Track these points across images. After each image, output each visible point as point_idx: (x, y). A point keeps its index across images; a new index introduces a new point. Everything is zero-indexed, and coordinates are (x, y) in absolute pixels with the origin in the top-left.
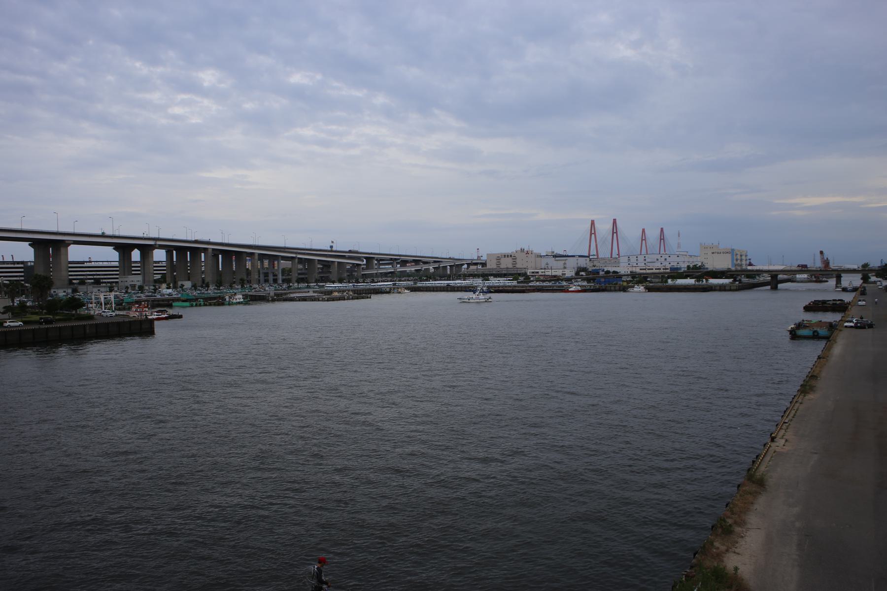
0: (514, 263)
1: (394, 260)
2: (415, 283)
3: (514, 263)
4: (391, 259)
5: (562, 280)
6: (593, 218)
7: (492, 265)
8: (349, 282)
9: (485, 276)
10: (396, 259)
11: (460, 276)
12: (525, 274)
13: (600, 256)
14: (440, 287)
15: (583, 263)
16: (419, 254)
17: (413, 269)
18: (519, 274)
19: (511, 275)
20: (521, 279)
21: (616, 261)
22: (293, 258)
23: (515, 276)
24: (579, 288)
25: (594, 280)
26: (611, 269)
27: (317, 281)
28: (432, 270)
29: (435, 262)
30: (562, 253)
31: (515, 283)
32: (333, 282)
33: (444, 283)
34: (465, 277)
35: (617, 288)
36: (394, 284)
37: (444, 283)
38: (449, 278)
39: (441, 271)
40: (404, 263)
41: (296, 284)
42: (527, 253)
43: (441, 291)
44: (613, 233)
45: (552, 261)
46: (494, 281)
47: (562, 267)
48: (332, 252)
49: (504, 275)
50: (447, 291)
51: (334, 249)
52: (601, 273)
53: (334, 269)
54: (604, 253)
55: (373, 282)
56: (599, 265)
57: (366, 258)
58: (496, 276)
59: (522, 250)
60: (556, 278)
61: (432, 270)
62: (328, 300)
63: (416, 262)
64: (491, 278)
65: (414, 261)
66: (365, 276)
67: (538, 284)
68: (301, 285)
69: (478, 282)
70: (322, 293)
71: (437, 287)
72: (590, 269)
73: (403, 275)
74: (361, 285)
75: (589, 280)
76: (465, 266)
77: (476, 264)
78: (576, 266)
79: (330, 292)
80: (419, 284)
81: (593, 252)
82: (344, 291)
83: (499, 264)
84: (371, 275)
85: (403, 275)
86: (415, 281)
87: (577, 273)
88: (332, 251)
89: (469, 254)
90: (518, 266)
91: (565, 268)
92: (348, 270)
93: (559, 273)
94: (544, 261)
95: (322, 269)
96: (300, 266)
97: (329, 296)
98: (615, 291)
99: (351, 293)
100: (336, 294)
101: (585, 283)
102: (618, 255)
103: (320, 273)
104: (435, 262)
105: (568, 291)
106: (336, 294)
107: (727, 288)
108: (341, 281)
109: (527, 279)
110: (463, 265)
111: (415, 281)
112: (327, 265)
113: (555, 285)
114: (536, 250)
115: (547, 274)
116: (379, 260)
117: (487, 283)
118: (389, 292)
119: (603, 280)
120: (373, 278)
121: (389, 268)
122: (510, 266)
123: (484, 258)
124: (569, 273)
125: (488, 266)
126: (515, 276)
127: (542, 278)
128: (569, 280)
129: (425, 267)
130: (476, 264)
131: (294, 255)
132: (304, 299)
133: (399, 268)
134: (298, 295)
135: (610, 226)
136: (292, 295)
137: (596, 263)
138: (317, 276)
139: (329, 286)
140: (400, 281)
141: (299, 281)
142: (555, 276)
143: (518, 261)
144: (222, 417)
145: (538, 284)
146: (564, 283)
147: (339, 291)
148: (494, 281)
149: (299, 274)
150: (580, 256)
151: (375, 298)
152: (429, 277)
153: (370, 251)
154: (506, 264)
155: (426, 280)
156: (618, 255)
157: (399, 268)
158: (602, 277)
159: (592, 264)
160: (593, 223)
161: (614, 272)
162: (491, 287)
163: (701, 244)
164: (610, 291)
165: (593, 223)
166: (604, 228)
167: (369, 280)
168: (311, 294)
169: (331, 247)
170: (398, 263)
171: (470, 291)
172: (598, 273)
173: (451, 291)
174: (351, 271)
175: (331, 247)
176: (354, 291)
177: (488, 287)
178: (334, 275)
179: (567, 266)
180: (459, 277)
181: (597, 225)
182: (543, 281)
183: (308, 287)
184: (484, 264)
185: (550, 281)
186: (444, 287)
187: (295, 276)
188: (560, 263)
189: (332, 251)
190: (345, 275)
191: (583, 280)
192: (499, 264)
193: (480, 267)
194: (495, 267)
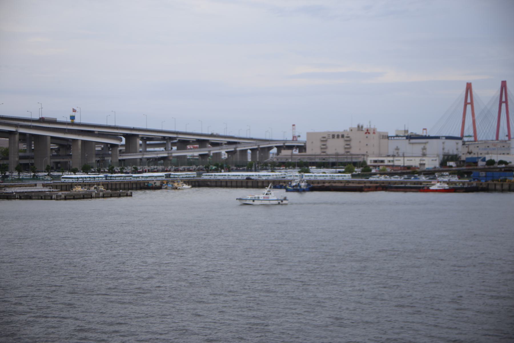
0: (348, 147)
1: (167, 139)
2: (199, 175)
3: (348, 147)
4: (164, 138)
5: (419, 173)
6: (469, 79)
7: (314, 150)
8: (99, 171)
9: (303, 166)
10: (171, 138)
11: (266, 164)
12: (363, 164)
13: (480, 137)
14: (237, 181)
15: (452, 147)
16: (205, 132)
17: (196, 154)
18: (355, 164)
19: (343, 164)
20: (358, 170)
21: (504, 146)
22: (11, 132)
23: (348, 166)
24: (446, 186)
25: (469, 173)
26: (497, 158)
27: (49, 169)
28: (225, 156)
29: (229, 143)
30: (420, 132)
31: (348, 176)
32: (75, 171)
33: (243, 175)
34: (274, 166)
35: (506, 186)
36: (168, 176)
37: (243, 175)
38: (249, 167)
39: (238, 158)
40: (183, 144)
41: (16, 174)
42: (368, 132)
43: (237, 187)
44: (501, 103)
45: (404, 145)
46: (317, 174)
47: (420, 153)
48: (73, 126)
49: (333, 165)
50: (247, 187)
51: (77, 121)
52: (481, 164)
53: (77, 152)
54: (486, 132)
55: (136, 171)
56: (477, 152)
57: (126, 136)
58: (320, 165)
59: (360, 128)
60: (410, 171)
61: (225, 156)
62: (65, 199)
63: (202, 143)
64: (313, 169)
65: (199, 141)
66: (123, 163)
67: (382, 178)
68: (24, 175)
69: (293, 175)
70: (56, 187)
71: (231, 181)
72: (463, 158)
73: (182, 163)
74: (118, 177)
75: (461, 174)
76: (275, 150)
77: (290, 147)
78: (441, 152)
79: (70, 186)
80: (206, 176)
81: (469, 131)
82: (90, 185)
83: (324, 147)
84: (133, 162)
85: (182, 163)
86: (200, 172)
87: (443, 164)
88: (73, 124)
89: (280, 133)
90: (353, 151)
91: (424, 155)
92: (98, 154)
93: (415, 162)
94: (392, 146)
95: (58, 150)
96: (23, 146)
97: (68, 193)
98: (502, 191)
99: (102, 188)
100: (79, 189)
101: (455, 179)
102: (509, 136)
103: (53, 156)
104: (229, 143)
105: (428, 190)
106: (79, 189)
107: (244, 184)
108: (86, 169)
109: (367, 170)
110: (270, 148)
111: (200, 172)
112: (65, 145)
113: (409, 180)
114: (381, 129)
115: (396, 163)
116: (145, 139)
117: (306, 176)
118: (159, 188)
119: (483, 174)
120: (136, 166)
121: (160, 152)
122: (341, 151)
123: (303, 138)
124: (431, 163)
125: (309, 151)
126: (348, 166)
127: (389, 170)
128: (430, 173)
129: (214, 150)
130: (290, 147)
131: (13, 129)
132: (28, 196)
133: (175, 152)
134: (18, 190)
135: (496, 91)
136: (9, 190)
137: (472, 148)
138: (50, 162)
139: (68, 176)
140: (176, 170)
141: (20, 168)
142: (409, 168)
143: (352, 144)
144: (8, 251)
145: (382, 178)
146: (423, 178)
147: (83, 185)
148: (317, 174)
149: (21, 158)
150: (448, 138)
151: (139, 196)
152: (220, 166)
153: (131, 126)
154: (336, 148)
155: (216, 170)
156: (509, 136)
157: (175, 152)
158: (482, 170)
159: (466, 150)
160: (469, 87)
161: (501, 162)
162: (313, 182)
163: (397, 147)
164: (495, 190)
165: (469, 87)
166: (486, 95)
167: (129, 169)
168: (39, 188)
169: (73, 118)
170: (173, 144)
171: (281, 187)
172: (476, 163)
173: (253, 187)
174: (102, 155)
175: (73, 118)
176: (107, 185)
177: (309, 182)
178: (76, 160)
179: (428, 152)
180: (265, 166)
181: (475, 90)
182: (391, 174)
183: (35, 178)
184: (302, 148)
185: (401, 174)
186: (242, 181)
187: (14, 160)
188: (417, 148)
189: (73, 124)
190: (94, 160)
191: (453, 173)
192: (324, 147)
193: (296, 152)
194: (318, 151)
